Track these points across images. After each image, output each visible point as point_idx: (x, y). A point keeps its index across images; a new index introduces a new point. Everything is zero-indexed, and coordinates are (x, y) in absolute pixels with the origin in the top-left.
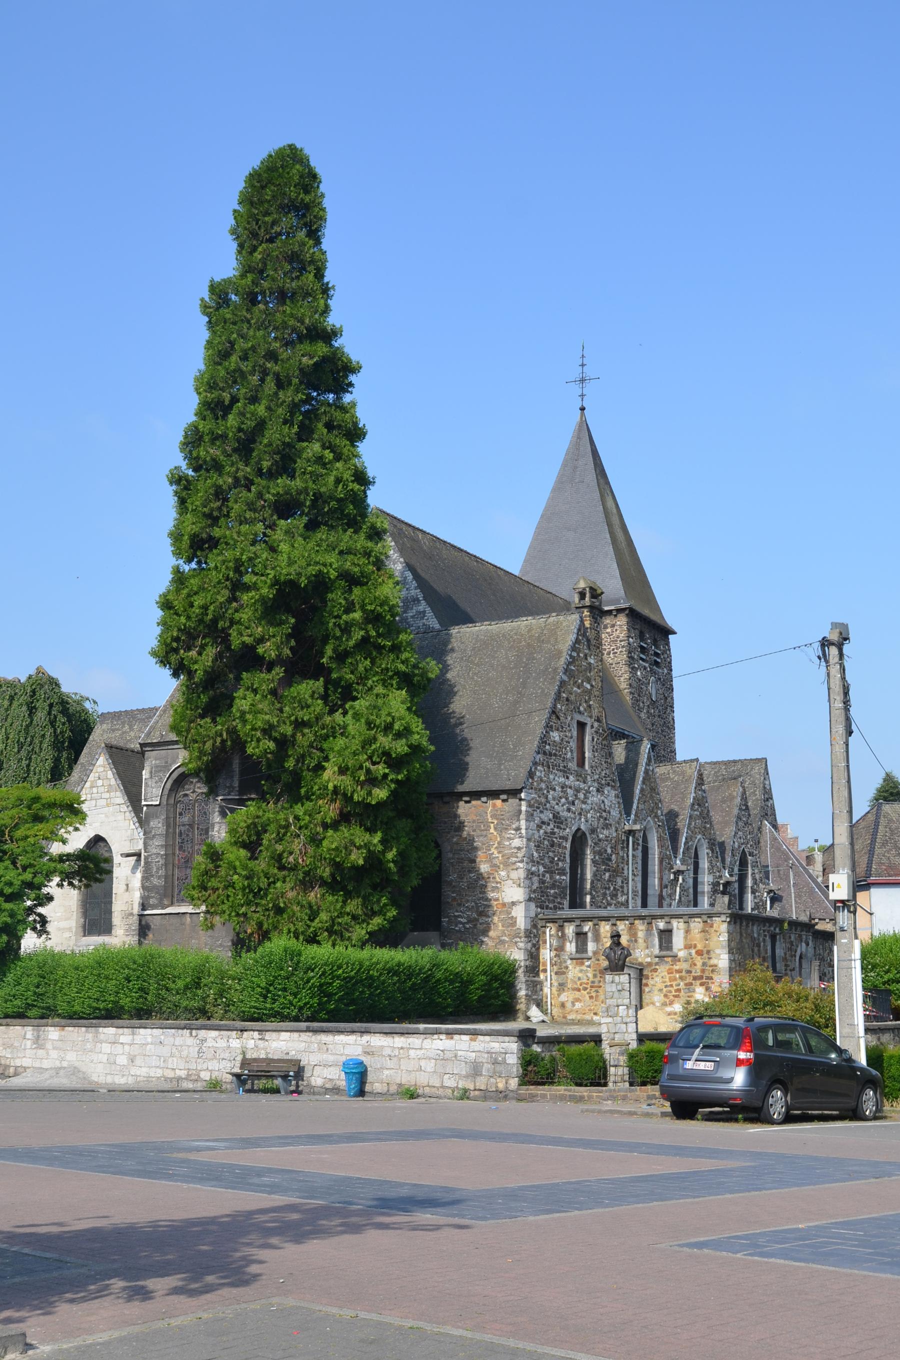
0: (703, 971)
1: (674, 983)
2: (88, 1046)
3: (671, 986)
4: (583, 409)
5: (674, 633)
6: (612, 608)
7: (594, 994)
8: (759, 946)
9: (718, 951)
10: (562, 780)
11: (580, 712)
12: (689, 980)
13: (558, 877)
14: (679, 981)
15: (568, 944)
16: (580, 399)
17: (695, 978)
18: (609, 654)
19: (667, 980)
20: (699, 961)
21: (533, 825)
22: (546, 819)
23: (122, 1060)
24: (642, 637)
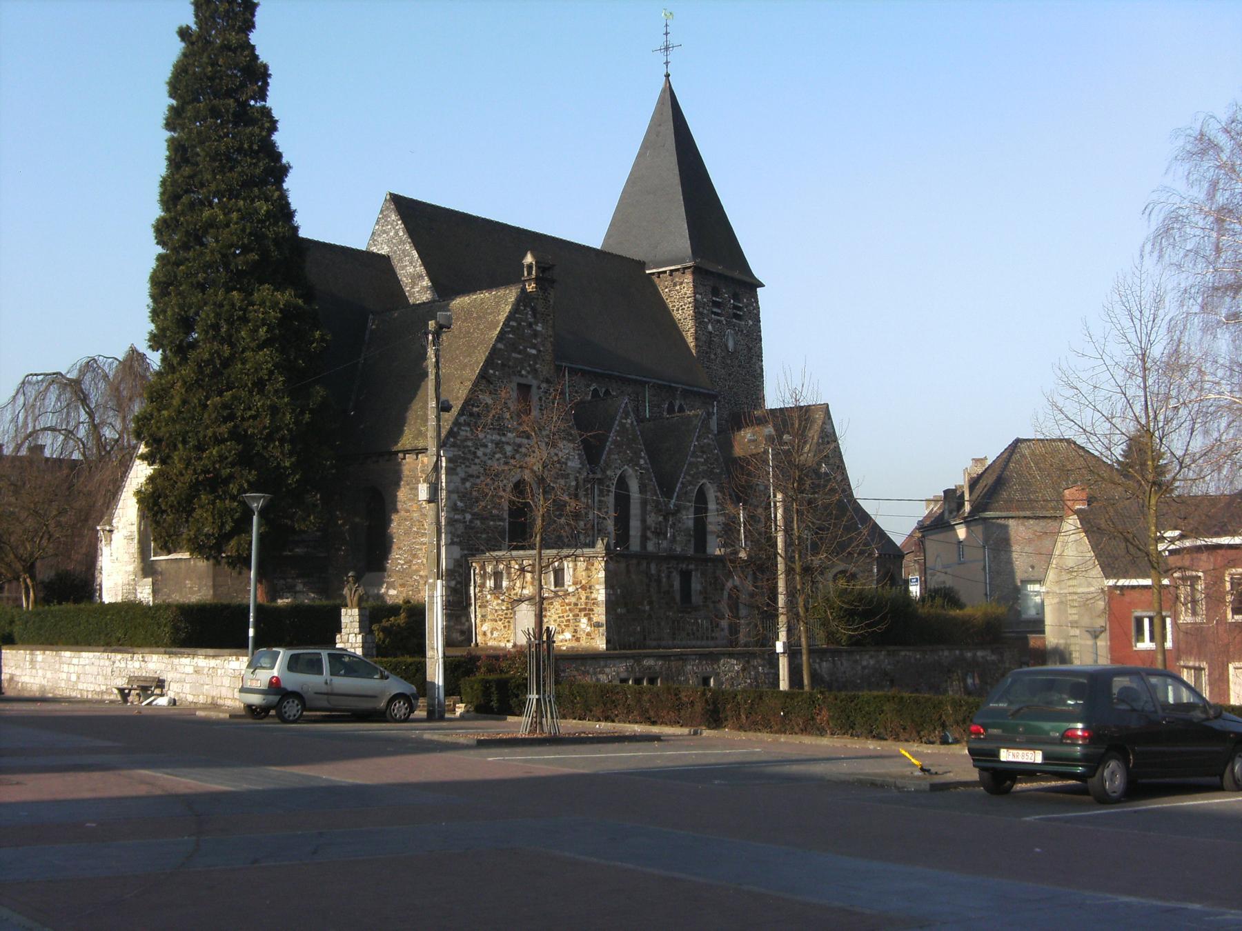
0: (586, 604)
1: (565, 615)
2: (57, 666)
3: (563, 617)
4: (667, 76)
5: (762, 285)
6: (679, 267)
7: (506, 624)
8: (659, 581)
9: (597, 587)
10: (496, 437)
11: (522, 376)
12: (577, 611)
13: (492, 523)
14: (569, 612)
15: (488, 581)
16: (665, 66)
17: (581, 610)
18: (678, 310)
19: (560, 611)
20: (583, 595)
21: (457, 479)
22: (475, 473)
23: (74, 678)
24: (715, 292)
